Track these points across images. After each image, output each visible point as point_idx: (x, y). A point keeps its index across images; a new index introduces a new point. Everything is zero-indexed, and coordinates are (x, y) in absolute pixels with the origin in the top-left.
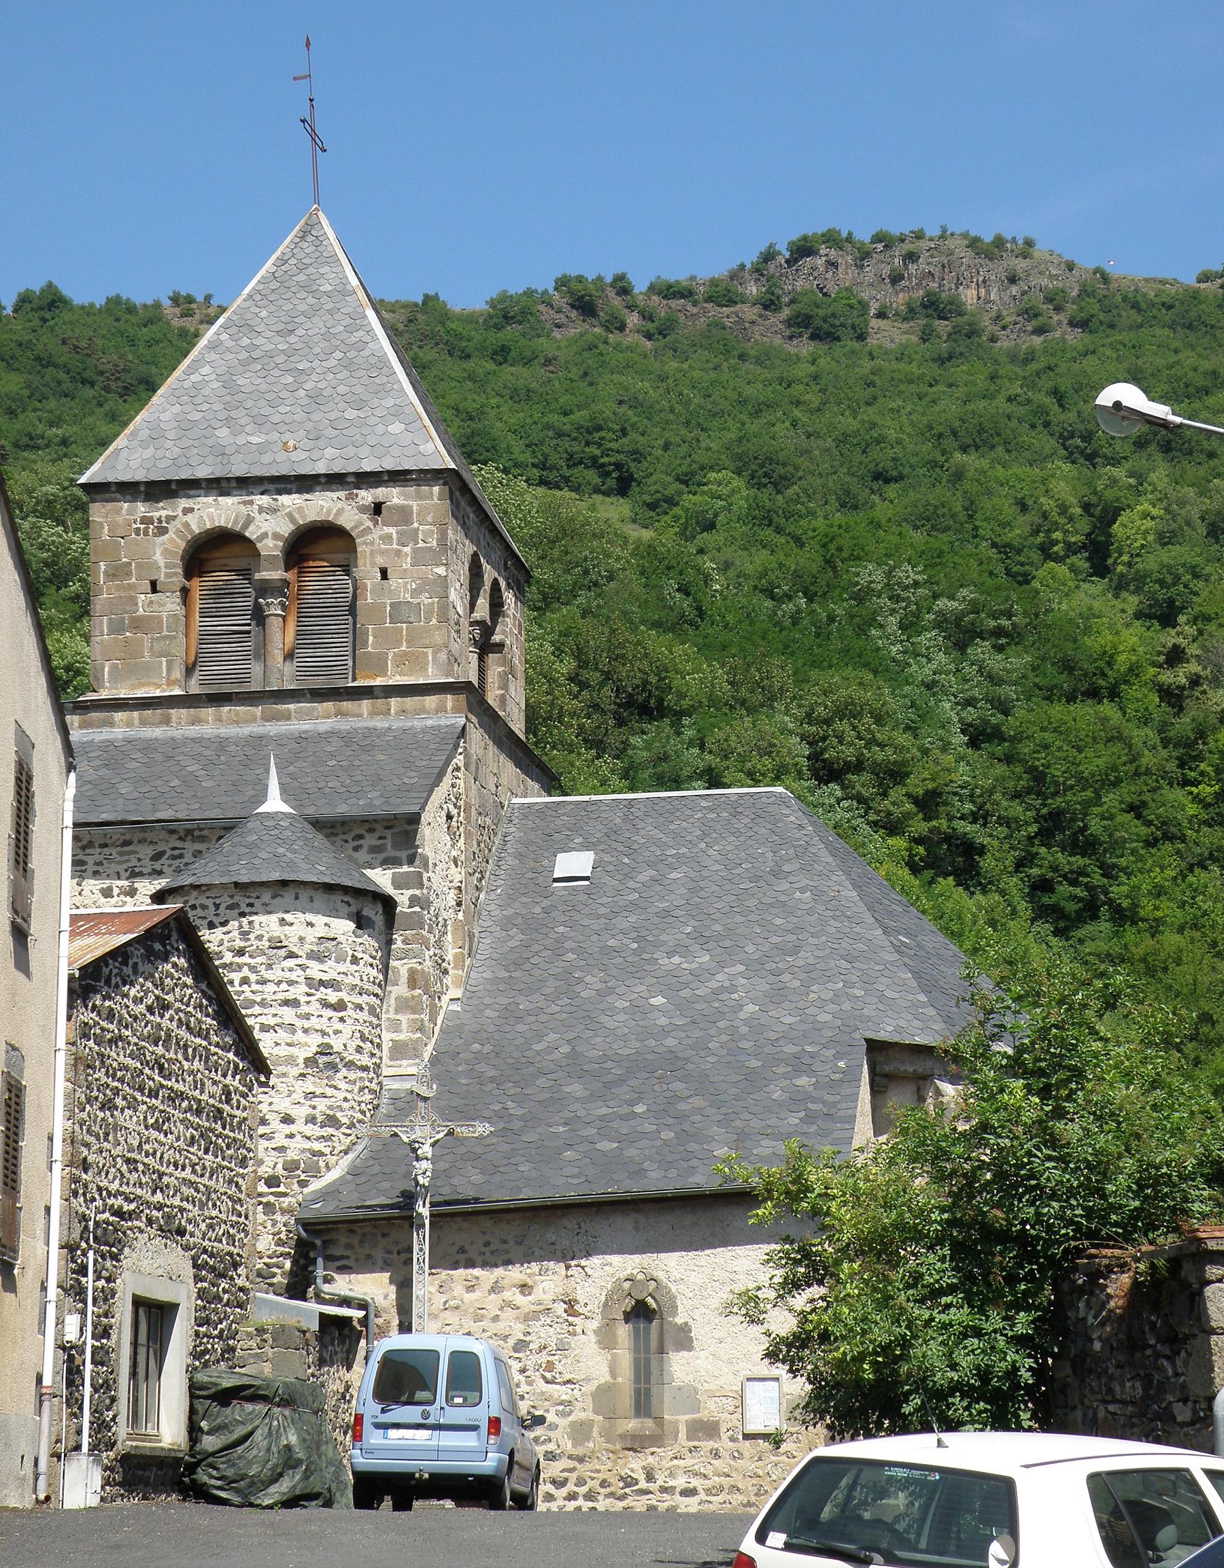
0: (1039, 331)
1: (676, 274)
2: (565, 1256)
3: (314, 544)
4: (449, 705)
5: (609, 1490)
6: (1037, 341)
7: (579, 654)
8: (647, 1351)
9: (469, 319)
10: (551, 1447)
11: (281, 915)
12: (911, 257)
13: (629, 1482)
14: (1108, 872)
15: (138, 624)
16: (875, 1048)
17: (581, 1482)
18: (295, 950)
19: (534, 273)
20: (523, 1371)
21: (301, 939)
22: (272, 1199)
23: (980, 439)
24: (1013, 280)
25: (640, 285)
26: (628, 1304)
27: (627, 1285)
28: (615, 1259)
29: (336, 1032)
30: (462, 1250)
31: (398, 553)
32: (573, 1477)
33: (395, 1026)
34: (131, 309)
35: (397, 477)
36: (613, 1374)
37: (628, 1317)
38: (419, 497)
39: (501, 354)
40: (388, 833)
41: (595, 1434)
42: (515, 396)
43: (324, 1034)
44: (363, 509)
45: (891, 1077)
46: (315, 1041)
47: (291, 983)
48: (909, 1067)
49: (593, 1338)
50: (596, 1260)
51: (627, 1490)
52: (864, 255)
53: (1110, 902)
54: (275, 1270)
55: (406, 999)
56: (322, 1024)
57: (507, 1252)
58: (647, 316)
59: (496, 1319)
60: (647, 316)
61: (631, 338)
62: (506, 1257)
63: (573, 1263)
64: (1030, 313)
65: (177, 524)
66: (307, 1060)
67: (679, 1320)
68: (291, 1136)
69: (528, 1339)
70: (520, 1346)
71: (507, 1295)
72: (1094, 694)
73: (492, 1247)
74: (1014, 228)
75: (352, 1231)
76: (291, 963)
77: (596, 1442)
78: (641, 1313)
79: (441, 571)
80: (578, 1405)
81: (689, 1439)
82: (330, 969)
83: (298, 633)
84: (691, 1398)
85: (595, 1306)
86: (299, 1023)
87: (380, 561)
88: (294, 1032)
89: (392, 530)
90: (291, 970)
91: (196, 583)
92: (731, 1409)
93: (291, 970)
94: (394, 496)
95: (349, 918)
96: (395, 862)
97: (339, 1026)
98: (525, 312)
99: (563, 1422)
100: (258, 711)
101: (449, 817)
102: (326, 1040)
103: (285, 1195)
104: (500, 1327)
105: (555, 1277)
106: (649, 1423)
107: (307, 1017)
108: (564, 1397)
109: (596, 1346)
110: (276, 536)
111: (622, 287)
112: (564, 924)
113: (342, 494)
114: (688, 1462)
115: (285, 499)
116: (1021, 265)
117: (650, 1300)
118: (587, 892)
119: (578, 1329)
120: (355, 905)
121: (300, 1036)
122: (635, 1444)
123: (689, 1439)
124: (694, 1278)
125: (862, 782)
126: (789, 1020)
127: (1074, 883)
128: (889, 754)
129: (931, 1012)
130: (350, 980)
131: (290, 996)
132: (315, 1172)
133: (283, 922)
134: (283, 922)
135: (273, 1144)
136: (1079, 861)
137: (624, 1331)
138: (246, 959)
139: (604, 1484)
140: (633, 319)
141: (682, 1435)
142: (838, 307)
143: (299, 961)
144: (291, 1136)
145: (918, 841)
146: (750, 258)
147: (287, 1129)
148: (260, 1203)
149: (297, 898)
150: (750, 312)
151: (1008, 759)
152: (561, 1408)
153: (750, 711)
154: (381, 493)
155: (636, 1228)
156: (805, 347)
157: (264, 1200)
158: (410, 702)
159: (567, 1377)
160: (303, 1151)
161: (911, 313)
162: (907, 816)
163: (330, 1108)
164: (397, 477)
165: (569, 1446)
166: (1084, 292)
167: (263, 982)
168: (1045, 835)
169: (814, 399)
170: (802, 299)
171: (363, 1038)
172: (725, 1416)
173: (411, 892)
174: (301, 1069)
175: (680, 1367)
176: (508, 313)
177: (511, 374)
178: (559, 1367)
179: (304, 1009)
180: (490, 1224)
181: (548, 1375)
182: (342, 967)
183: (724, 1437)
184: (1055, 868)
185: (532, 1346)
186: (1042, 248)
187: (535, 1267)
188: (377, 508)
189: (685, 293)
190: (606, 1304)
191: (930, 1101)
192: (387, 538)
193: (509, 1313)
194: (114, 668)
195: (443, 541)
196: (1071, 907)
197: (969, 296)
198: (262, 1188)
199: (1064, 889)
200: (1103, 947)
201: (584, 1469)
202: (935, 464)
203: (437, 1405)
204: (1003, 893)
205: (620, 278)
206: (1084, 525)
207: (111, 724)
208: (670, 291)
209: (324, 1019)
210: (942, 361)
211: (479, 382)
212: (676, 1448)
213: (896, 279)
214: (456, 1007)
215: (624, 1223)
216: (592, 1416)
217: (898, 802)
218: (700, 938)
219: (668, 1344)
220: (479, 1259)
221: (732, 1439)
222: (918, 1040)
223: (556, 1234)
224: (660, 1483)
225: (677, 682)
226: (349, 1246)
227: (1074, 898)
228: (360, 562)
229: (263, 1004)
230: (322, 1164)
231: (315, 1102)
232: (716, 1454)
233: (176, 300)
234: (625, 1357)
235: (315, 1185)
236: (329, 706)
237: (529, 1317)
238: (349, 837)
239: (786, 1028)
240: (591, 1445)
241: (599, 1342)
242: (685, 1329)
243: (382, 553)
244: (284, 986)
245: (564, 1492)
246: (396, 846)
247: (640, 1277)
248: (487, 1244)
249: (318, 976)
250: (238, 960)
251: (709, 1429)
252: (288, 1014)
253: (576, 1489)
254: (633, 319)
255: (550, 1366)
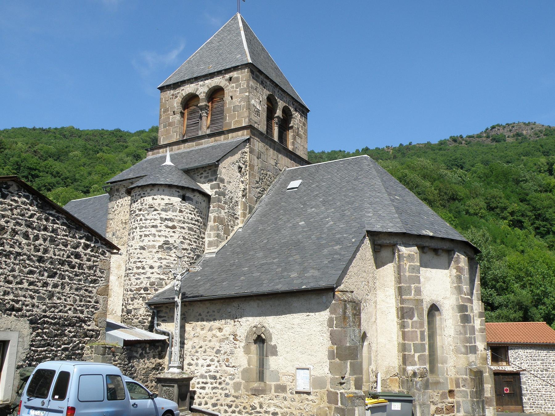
0: (538, 137)
1: (471, 134)
2: (234, 317)
3: (216, 93)
4: (245, 133)
5: (246, 410)
6: (538, 139)
7: (440, 189)
8: (263, 355)
9: (435, 145)
10: (227, 392)
11: (153, 197)
12: (513, 127)
13: (253, 408)
14: (551, 225)
15: (170, 124)
16: (372, 234)
17: (237, 407)
18: (157, 208)
19: (446, 136)
20: (218, 361)
21: (159, 204)
22: (145, 295)
23: (527, 154)
24: (532, 129)
25: (464, 137)
26: (255, 336)
27: (254, 329)
28: (250, 319)
29: (171, 236)
30: (200, 315)
31: (235, 91)
32: (234, 404)
33: (209, 236)
34: (379, 149)
35: (235, 68)
36: (249, 365)
37: (256, 341)
38: (242, 73)
39: (440, 149)
40: (210, 172)
41: (242, 388)
42: (442, 155)
43: (166, 237)
44: (226, 80)
45: (381, 246)
46: (162, 239)
47: (155, 220)
48: (387, 241)
49: (242, 350)
50: (244, 319)
51: (253, 411)
52: (504, 127)
53: (552, 231)
54: (145, 321)
55: (213, 226)
56: (166, 233)
57: (215, 315)
58: (466, 141)
59: (210, 341)
60: (466, 141)
61: (463, 145)
62: (214, 317)
63: (236, 320)
64: (536, 134)
65: (180, 94)
66: (160, 247)
67: (273, 343)
68: (152, 273)
69: (220, 349)
70: (218, 352)
71: (214, 332)
72: (546, 191)
73: (210, 314)
74: (532, 120)
75: (167, 307)
76: (155, 212)
77: (242, 391)
78: (260, 340)
79: (247, 94)
80: (237, 376)
81: (275, 392)
82: (170, 214)
83: (211, 121)
84: (276, 375)
85: (243, 337)
86: (157, 233)
87: (231, 94)
88: (155, 237)
89: (234, 85)
90: (155, 215)
91: (186, 112)
92: (291, 380)
93: (155, 215)
94: (235, 74)
95: (179, 196)
96: (211, 181)
97: (173, 234)
98: (445, 143)
99: (231, 382)
100: (194, 143)
101: (240, 168)
102: (167, 239)
103: (149, 294)
104: (211, 344)
105: (230, 326)
106: (262, 384)
107: (160, 231)
108: (232, 373)
109: (243, 353)
110: (204, 92)
111: (461, 137)
112: (285, 202)
113: (221, 77)
114: (275, 401)
115: (207, 82)
116: (534, 126)
117: (262, 335)
118: (295, 192)
119: (237, 346)
120: (182, 193)
121: (157, 238)
122: (256, 393)
123: (275, 392)
124: (279, 326)
125: (498, 211)
126: (342, 226)
127: (544, 227)
128: (503, 205)
129: (399, 220)
130: (178, 218)
131: (154, 224)
132: (161, 286)
133: (153, 199)
134: (153, 199)
135: (146, 276)
136: (545, 223)
137: (254, 348)
138: (142, 212)
139: (245, 408)
140: (464, 142)
141: (273, 390)
142: (500, 136)
143: (158, 212)
144: (152, 273)
145: (511, 221)
146: (484, 130)
147: (151, 271)
148: (141, 297)
149: (158, 190)
150: (484, 139)
151: (528, 205)
152: (231, 377)
153: (474, 198)
154: (231, 74)
155: (258, 306)
156: (494, 143)
157: (142, 296)
158: (234, 134)
159: (233, 365)
160: (157, 278)
161: (514, 136)
162: (508, 216)
163: (168, 263)
164: (235, 68)
165: (233, 392)
166: (546, 130)
167: (146, 220)
168: (537, 219)
169: (496, 151)
170: (494, 136)
171: (184, 238)
172: (289, 383)
173: (215, 190)
174: (157, 249)
175: (273, 362)
176: (442, 143)
177: (441, 152)
178: (231, 361)
179: (159, 228)
180: (209, 305)
181: (227, 364)
182: (174, 214)
183: (288, 392)
184: (540, 225)
185: (222, 352)
186: (537, 123)
187: (223, 321)
188: (230, 79)
189: (472, 137)
190: (247, 336)
191: (396, 254)
192: (233, 87)
193: (215, 339)
194: (164, 138)
195: (248, 86)
196: (544, 232)
197: (524, 132)
198: (142, 291)
199: (542, 229)
200: (551, 239)
201: (238, 401)
202: (518, 159)
203: (48, 399)
204: (529, 230)
205: (461, 135)
206: (547, 167)
207: (159, 153)
208: (470, 137)
209: (167, 232)
210: (520, 143)
211: (436, 154)
212: (271, 395)
213: (510, 131)
214: (240, 230)
215: (254, 304)
216: (241, 381)
217: (506, 213)
218: (324, 203)
219: (269, 354)
220: (205, 318)
221: (292, 393)
222: (389, 230)
223: (232, 308)
224: (264, 409)
225: (459, 193)
226: (166, 313)
227: (544, 230)
228: (225, 96)
229: (146, 227)
230: (164, 283)
231: (162, 261)
232: (285, 399)
233: (387, 147)
234: (254, 357)
235: (161, 290)
236: (213, 139)
237: (221, 341)
238: (199, 174)
239: (339, 229)
240: (240, 392)
241: (244, 351)
242: (275, 347)
243: (231, 92)
244: (153, 221)
245: (231, 410)
246: (212, 175)
247: (259, 326)
248: (208, 312)
249: (164, 217)
250: (140, 213)
251: (282, 388)
252: (153, 230)
253: (235, 409)
254: (464, 142)
255: (228, 360)
